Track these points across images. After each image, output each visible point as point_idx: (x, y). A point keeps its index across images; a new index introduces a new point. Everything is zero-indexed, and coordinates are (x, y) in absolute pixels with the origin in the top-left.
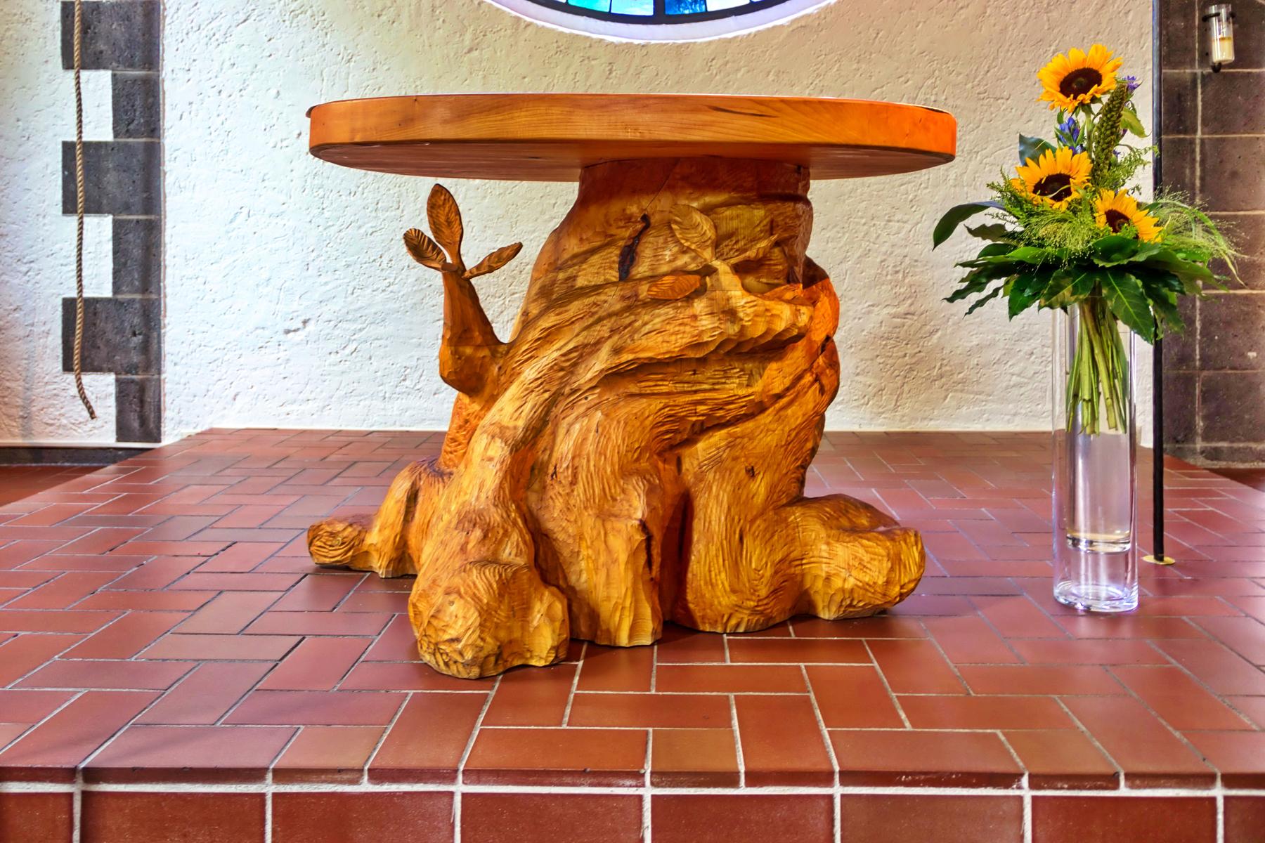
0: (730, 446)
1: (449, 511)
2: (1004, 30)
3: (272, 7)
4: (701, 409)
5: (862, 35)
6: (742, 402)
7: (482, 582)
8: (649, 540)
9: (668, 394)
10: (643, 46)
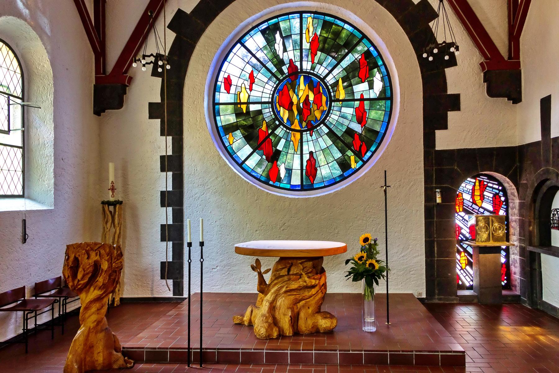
0: (305, 303)
4: (300, 297)
6: (307, 296)
7: (266, 325)
8: (291, 319)
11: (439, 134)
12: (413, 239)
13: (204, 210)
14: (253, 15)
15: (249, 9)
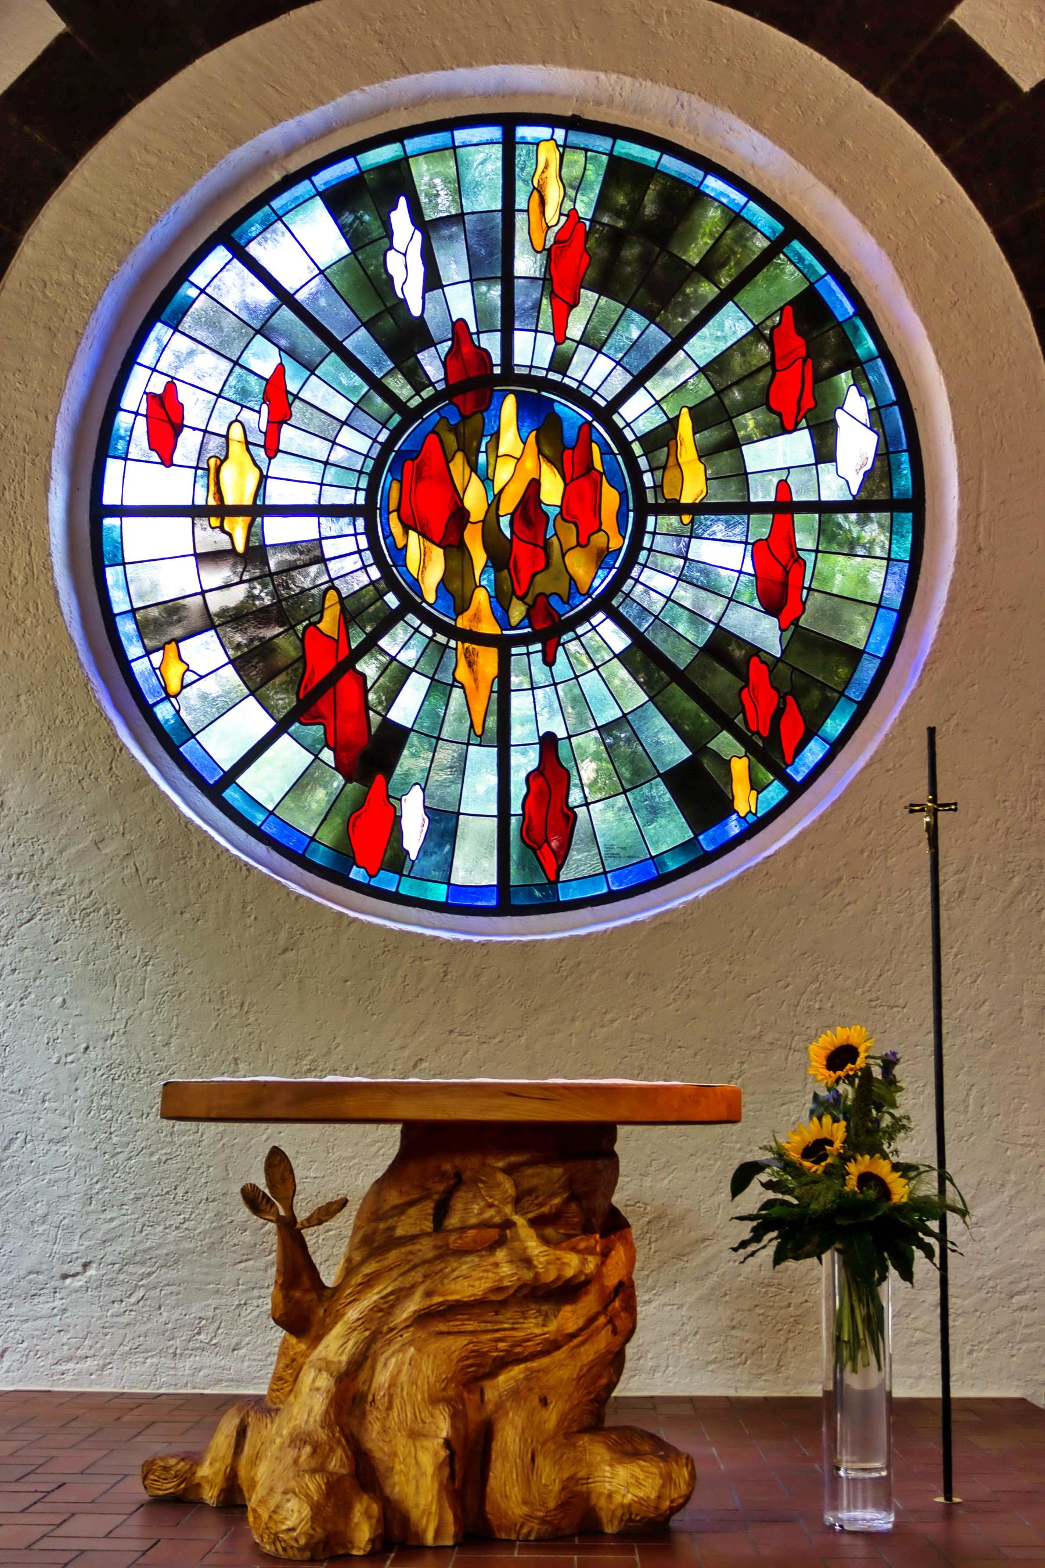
0: (527, 1379)
1: (281, 1435)
2: (898, 929)
3: (61, 904)
4: (502, 1345)
5: (735, 932)
6: (538, 1340)
7: (314, 1485)
8: (451, 1459)
9: (473, 1333)
10: (483, 945)
12: (1024, 1140)
13: (33, 996)
14: (291, 116)
15: (269, 89)
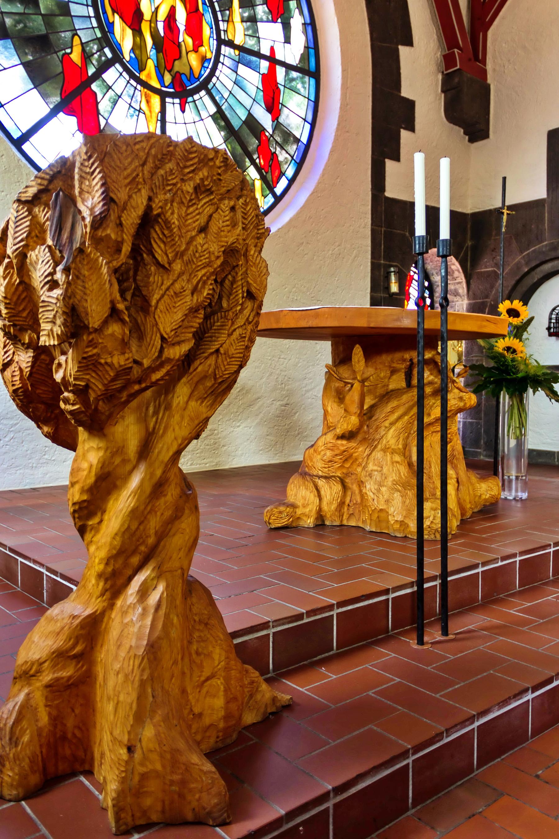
11: (389, 164)
